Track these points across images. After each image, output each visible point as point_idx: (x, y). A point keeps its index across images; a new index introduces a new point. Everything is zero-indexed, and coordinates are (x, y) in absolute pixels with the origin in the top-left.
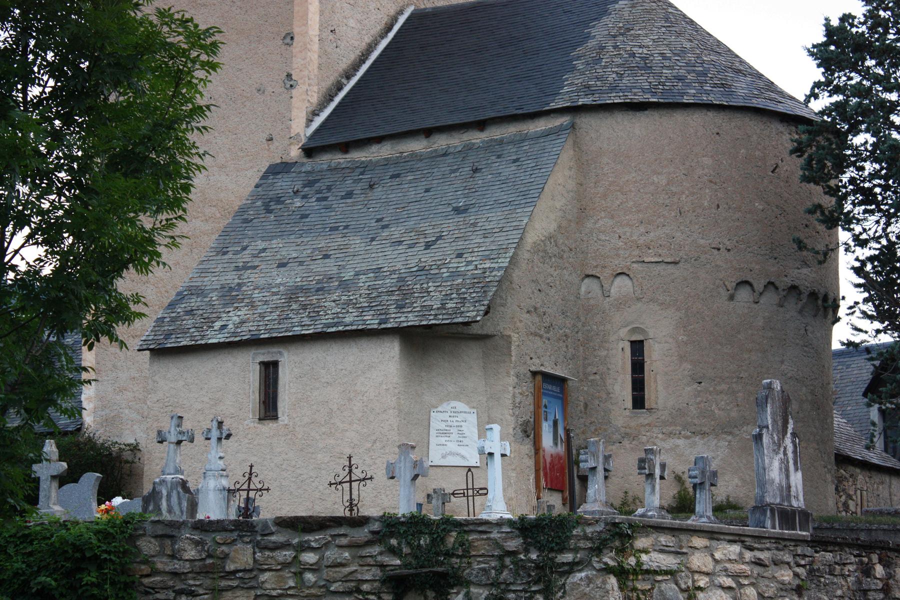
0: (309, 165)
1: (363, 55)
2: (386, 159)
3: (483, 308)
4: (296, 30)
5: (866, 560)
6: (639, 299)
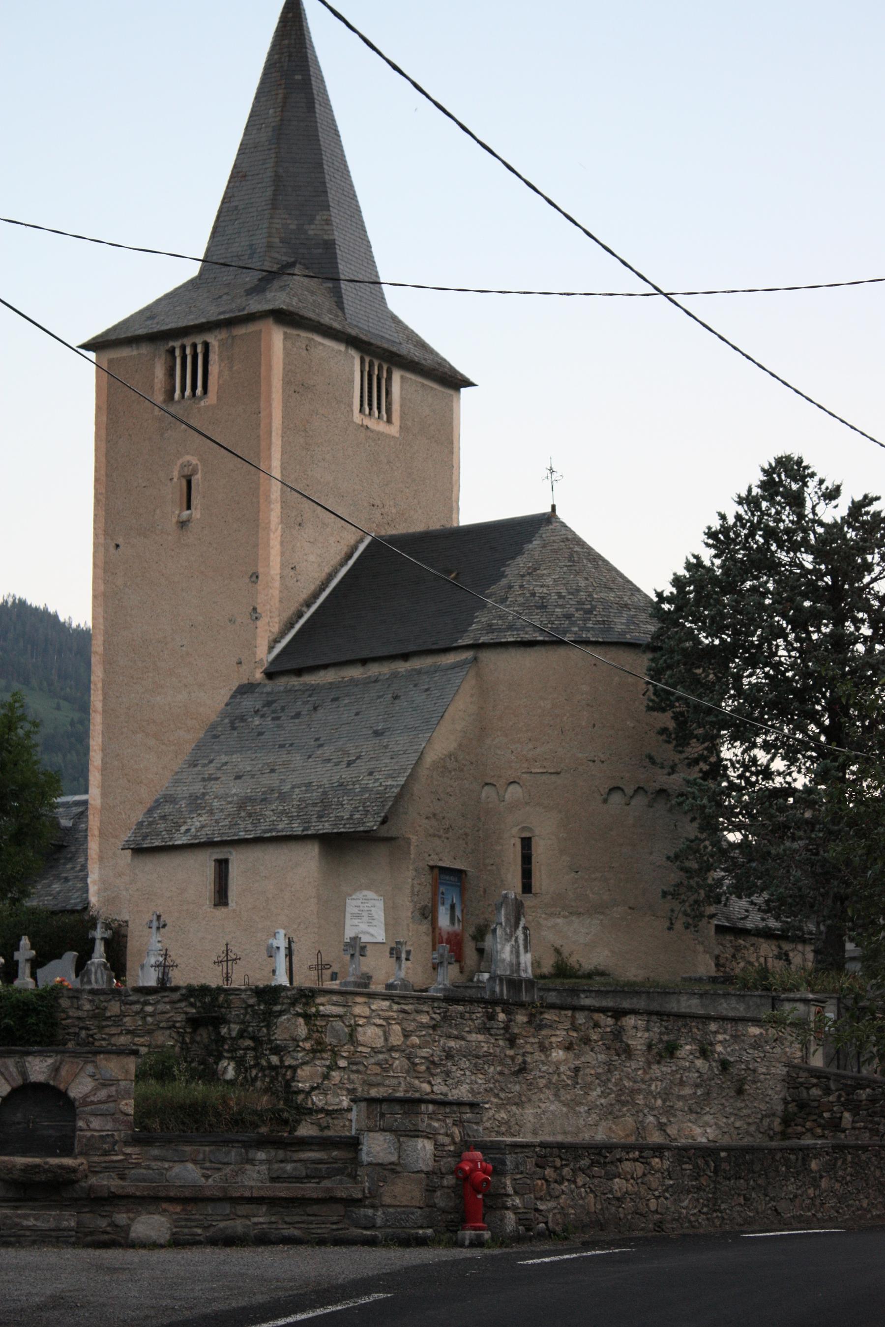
0: (270, 686)
1: (323, 584)
2: (331, 683)
3: (379, 819)
4: (261, 570)
5: (490, 1010)
6: (527, 803)
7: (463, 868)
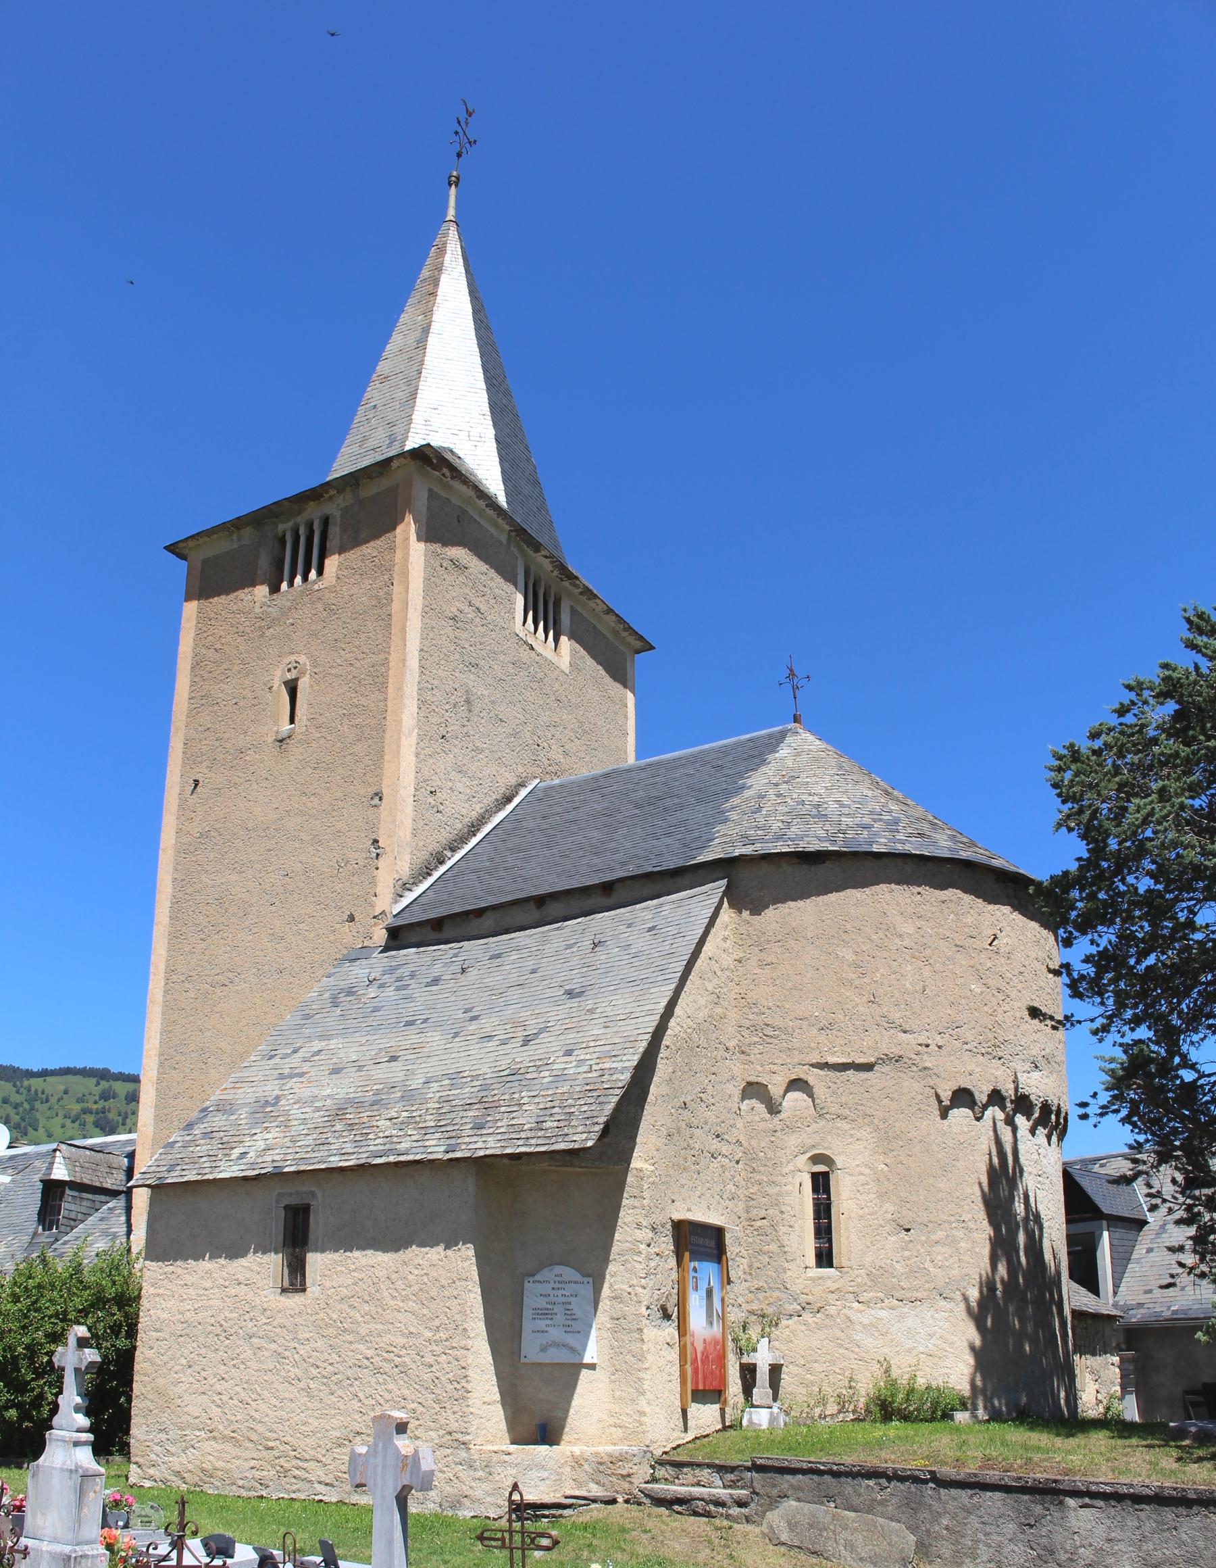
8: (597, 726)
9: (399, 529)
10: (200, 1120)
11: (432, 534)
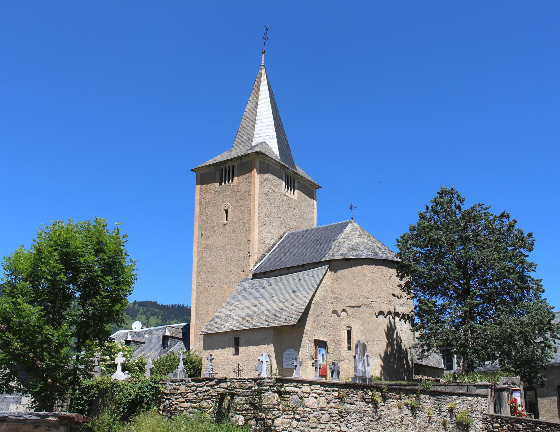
7: (324, 339)
8: (306, 214)
9: (252, 172)
10: (213, 320)
11: (260, 172)
